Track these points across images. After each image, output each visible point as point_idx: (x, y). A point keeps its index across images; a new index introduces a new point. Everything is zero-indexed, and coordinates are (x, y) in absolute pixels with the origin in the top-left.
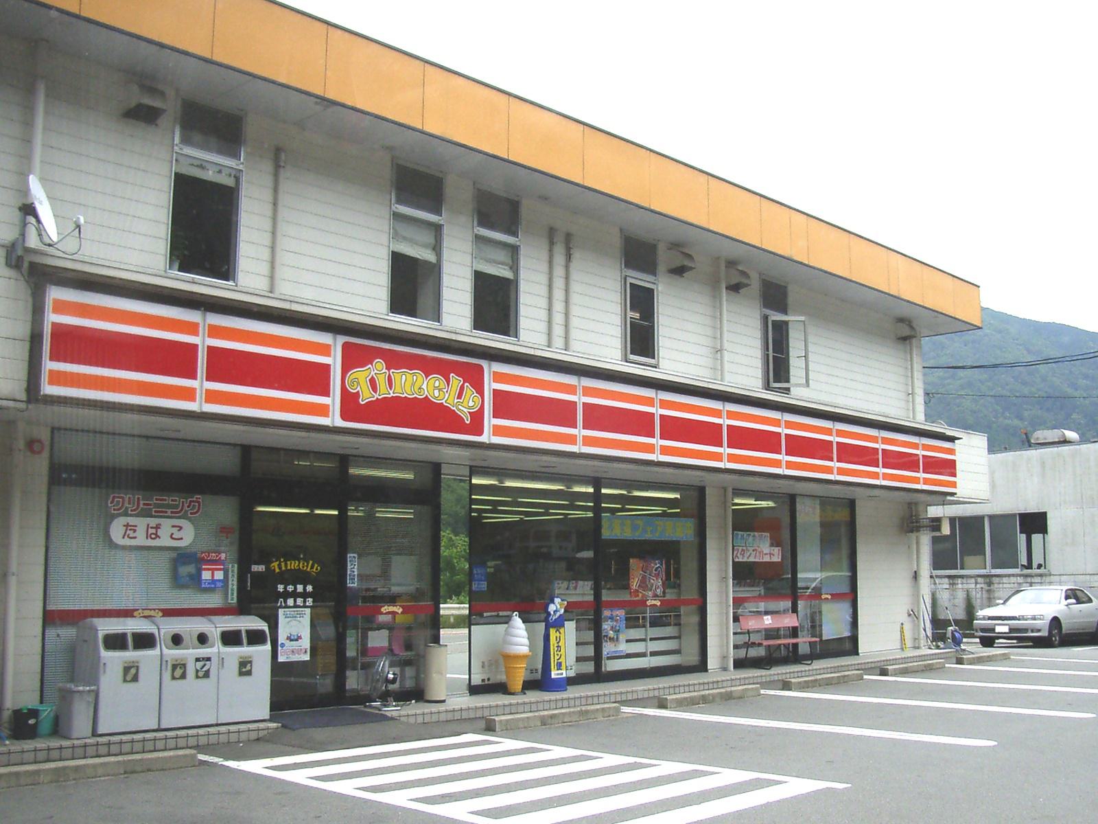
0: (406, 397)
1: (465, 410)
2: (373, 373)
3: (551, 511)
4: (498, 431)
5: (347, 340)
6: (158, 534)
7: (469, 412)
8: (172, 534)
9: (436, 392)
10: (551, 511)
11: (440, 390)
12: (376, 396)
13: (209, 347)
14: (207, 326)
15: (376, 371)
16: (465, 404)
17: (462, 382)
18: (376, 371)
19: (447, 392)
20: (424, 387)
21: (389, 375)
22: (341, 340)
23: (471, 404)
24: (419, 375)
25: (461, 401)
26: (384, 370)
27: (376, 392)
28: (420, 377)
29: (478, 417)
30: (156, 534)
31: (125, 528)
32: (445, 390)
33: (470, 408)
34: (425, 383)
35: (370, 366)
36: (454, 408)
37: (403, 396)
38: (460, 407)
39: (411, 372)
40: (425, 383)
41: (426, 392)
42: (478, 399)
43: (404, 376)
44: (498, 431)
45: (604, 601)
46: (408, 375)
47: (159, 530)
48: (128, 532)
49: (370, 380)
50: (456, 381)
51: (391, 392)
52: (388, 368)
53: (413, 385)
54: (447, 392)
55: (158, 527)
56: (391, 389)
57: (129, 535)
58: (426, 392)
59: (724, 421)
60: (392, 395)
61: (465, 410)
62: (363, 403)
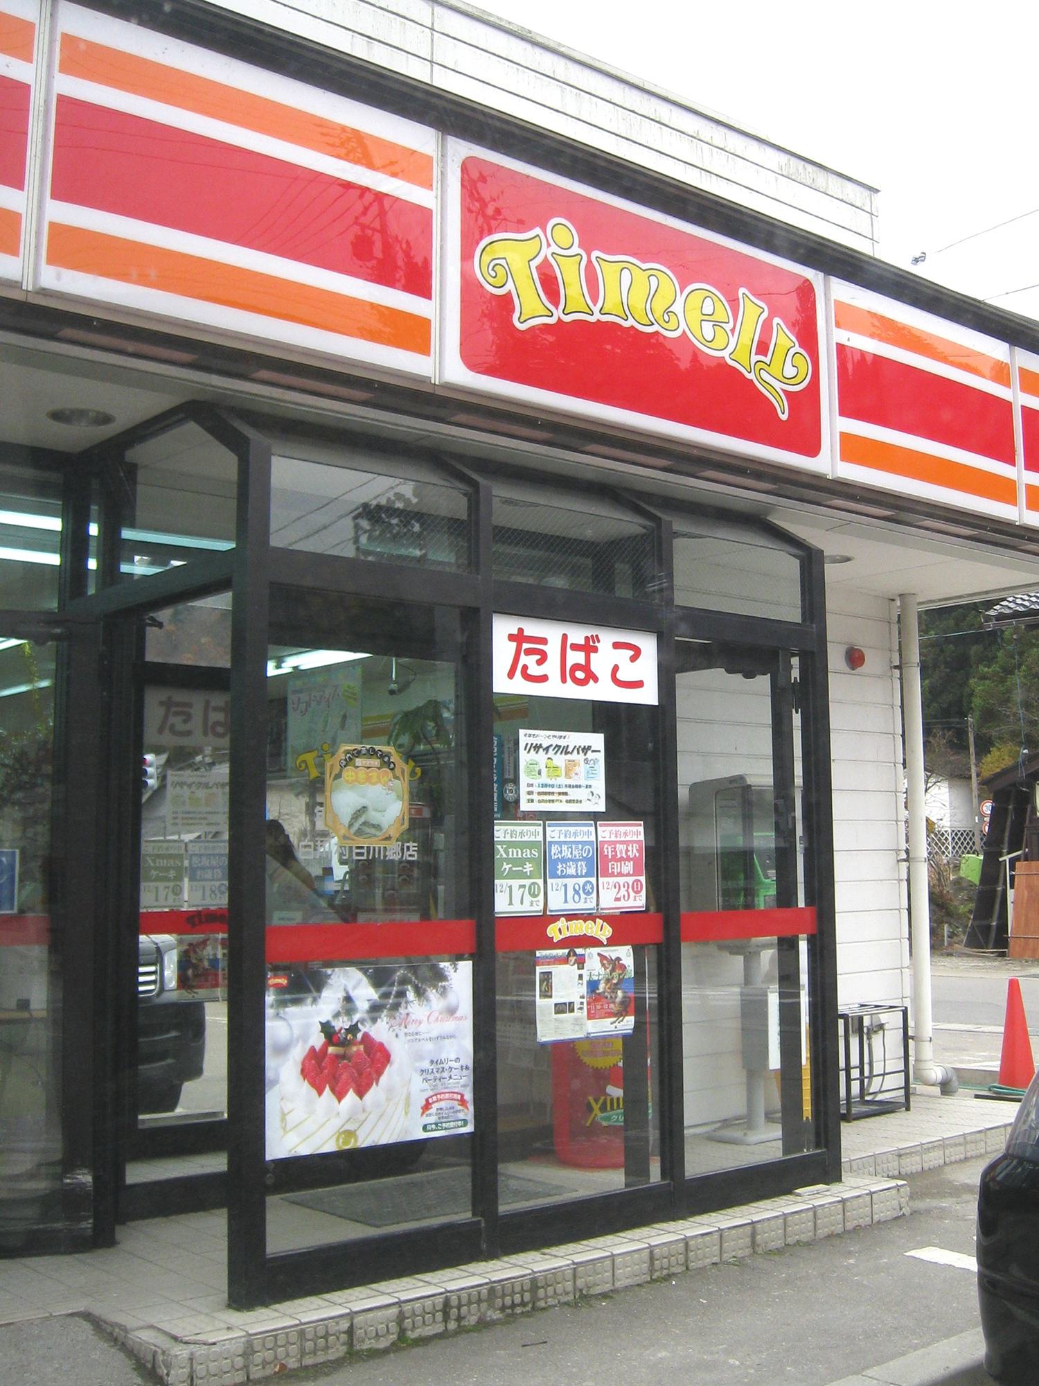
0: (632, 327)
1: (777, 385)
2: (546, 252)
3: (797, 719)
4: (853, 449)
5: (471, 154)
6: (593, 668)
7: (784, 391)
8: (616, 669)
9: (707, 327)
10: (797, 719)
11: (716, 324)
12: (558, 314)
13: (62, 99)
14: (58, 37)
15: (554, 248)
16: (775, 369)
17: (765, 315)
18: (554, 248)
19: (733, 331)
20: (678, 308)
21: (589, 262)
22: (461, 149)
23: (790, 371)
24: (666, 281)
25: (767, 360)
26: (576, 249)
27: (556, 305)
28: (664, 280)
29: (806, 401)
30: (586, 668)
31: (514, 644)
32: (729, 327)
33: (785, 380)
34: (680, 300)
35: (538, 231)
36: (750, 376)
37: (626, 324)
38: (764, 375)
39: (645, 266)
40: (680, 300)
41: (683, 326)
42: (804, 364)
43: (626, 273)
44: (853, 449)
45: (615, 1166)
46: (635, 271)
47: (593, 655)
48: (524, 659)
49: (538, 268)
50: (753, 311)
51: (596, 310)
52: (587, 246)
53: (651, 297)
54: (733, 331)
55: (588, 648)
56: (595, 301)
57: (525, 667)
58: (683, 326)
59: (1019, 472)
60: (597, 316)
61: (777, 385)
62: (522, 327)
